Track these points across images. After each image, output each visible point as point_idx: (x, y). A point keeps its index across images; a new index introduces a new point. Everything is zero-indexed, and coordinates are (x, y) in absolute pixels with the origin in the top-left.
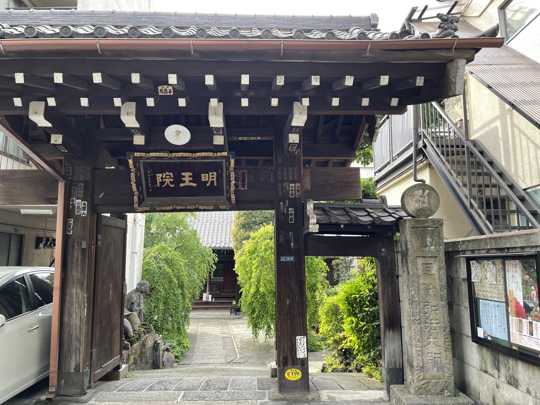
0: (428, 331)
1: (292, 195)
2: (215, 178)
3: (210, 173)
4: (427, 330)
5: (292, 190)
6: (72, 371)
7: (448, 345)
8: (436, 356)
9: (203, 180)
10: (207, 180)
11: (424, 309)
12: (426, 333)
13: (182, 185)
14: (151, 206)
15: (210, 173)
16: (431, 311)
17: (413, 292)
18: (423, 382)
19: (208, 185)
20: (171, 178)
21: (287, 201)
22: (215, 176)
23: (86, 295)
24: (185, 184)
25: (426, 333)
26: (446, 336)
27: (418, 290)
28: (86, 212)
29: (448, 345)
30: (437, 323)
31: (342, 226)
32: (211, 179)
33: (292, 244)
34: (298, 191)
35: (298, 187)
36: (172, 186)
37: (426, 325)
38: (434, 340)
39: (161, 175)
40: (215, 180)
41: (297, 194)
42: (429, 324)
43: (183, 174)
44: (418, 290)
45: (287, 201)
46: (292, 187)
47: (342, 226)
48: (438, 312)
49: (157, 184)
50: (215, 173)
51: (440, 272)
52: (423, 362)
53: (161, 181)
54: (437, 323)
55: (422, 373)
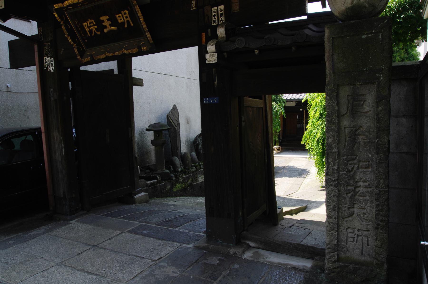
0: (351, 198)
1: (215, 22)
2: (129, 17)
3: (123, 12)
4: (350, 195)
5: (215, 16)
6: (62, 196)
7: (381, 221)
8: (360, 233)
9: (120, 21)
10: (122, 21)
11: (346, 165)
12: (348, 199)
13: (106, 31)
14: (91, 56)
15: (123, 12)
16: (358, 168)
17: (330, 140)
18: (336, 265)
19: (126, 26)
20: (94, 25)
21: (209, 30)
22: (127, 15)
23: (62, 138)
24: (108, 29)
25: (348, 199)
26: (380, 207)
27: (339, 136)
28: (53, 68)
29: (381, 221)
30: (366, 187)
31: (257, 52)
32: (126, 20)
33: (216, 82)
34: (221, 15)
35: (221, 10)
36: (99, 33)
37: (349, 188)
38: (360, 211)
39: (86, 23)
40: (129, 19)
41: (220, 19)
42: (353, 188)
43: (101, 18)
44: (339, 136)
45: (209, 30)
46: (215, 12)
47: (257, 52)
48: (370, 170)
49: (87, 34)
50: (127, 12)
51: (377, 107)
52: (338, 239)
53: (88, 29)
54: (366, 187)
55: (336, 253)
